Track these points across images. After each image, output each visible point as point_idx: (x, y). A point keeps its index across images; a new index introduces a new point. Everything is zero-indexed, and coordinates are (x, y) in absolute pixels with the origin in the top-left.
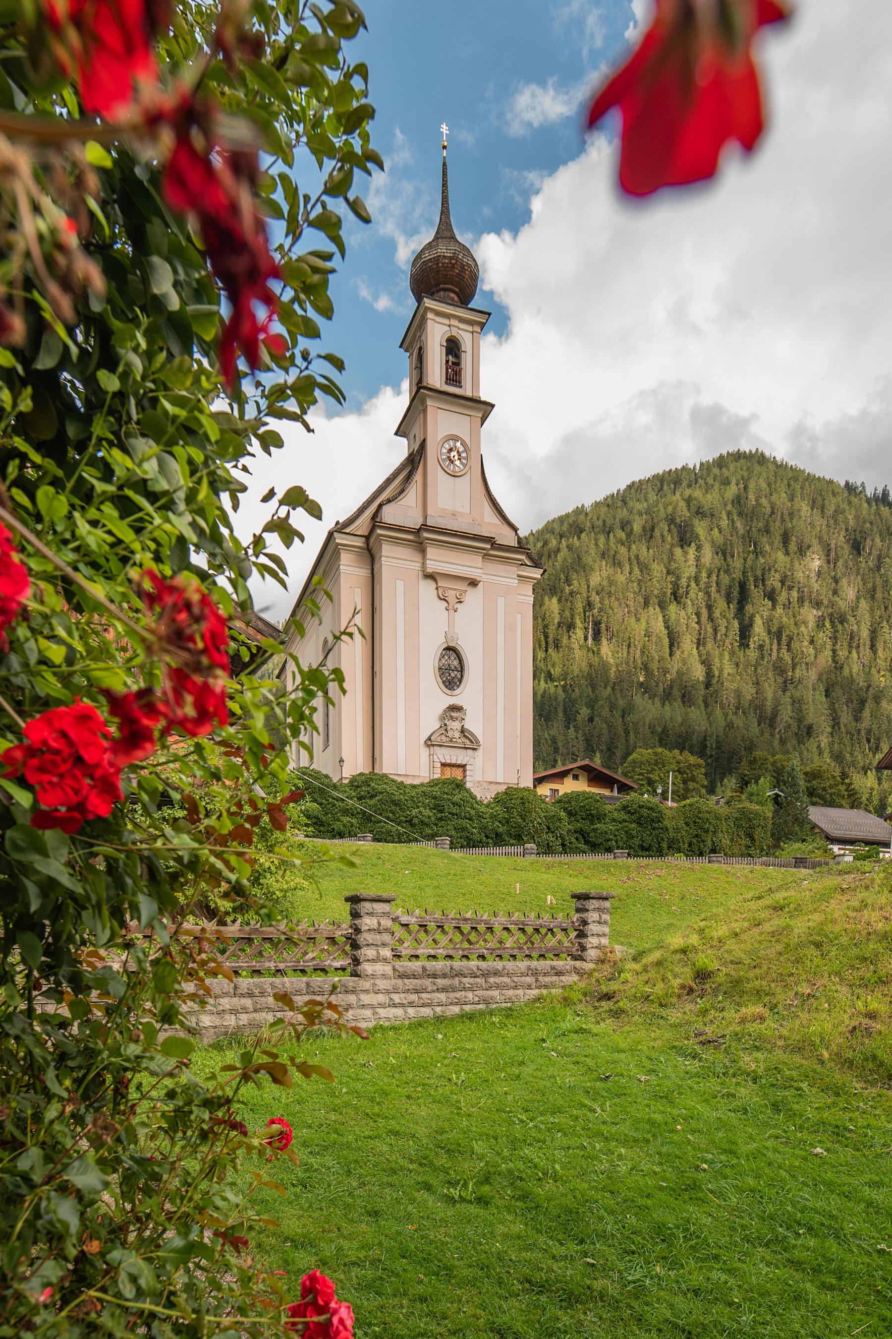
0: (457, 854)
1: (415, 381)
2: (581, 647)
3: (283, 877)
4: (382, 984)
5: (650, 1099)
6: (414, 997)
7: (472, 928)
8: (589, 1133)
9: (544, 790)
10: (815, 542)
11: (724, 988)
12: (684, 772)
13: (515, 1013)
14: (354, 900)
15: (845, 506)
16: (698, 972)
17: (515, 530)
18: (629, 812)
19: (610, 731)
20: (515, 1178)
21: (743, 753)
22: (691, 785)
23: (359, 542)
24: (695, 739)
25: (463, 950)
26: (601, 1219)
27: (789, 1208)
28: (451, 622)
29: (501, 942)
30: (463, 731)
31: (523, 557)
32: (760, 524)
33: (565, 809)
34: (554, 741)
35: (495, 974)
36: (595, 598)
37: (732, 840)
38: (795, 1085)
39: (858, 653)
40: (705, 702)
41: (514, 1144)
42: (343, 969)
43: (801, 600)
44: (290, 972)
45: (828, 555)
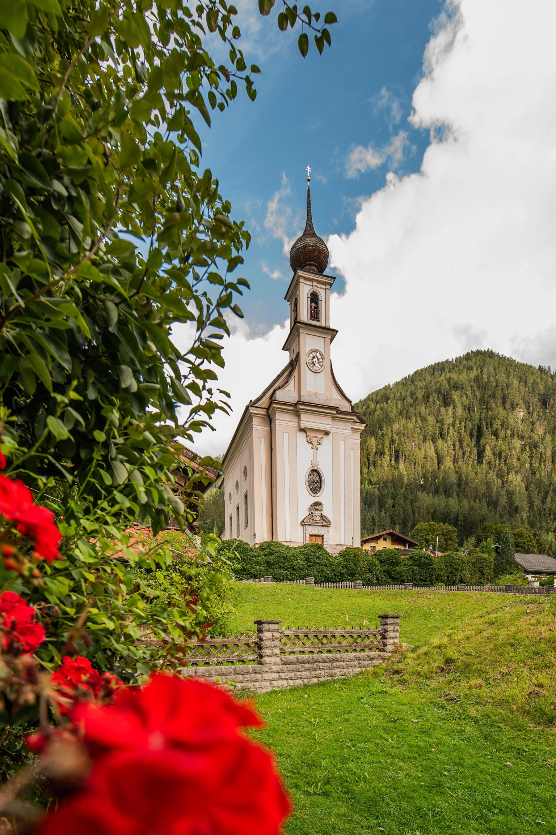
0: (317, 588)
1: (293, 319)
2: (388, 466)
3: (222, 605)
4: (275, 668)
5: (418, 733)
6: (292, 675)
7: (324, 636)
8: (384, 753)
9: (367, 547)
10: (521, 402)
11: (460, 669)
12: (446, 535)
13: (347, 682)
14: (259, 623)
15: (539, 380)
16: (447, 660)
17: (350, 402)
18: (414, 560)
19: (404, 513)
20: (343, 781)
21: (479, 523)
22: (450, 542)
23: (263, 412)
24: (452, 516)
25: (319, 648)
26: (388, 804)
27: (490, 799)
28: (314, 456)
29: (339, 643)
30: (322, 516)
31: (354, 418)
32: (490, 392)
33: (378, 559)
34: (373, 518)
35: (336, 661)
36: (396, 437)
37: (471, 574)
38: (497, 724)
39: (545, 465)
40: (458, 494)
41: (344, 760)
42: (254, 660)
43: (513, 435)
44: (225, 663)
45: (528, 409)
